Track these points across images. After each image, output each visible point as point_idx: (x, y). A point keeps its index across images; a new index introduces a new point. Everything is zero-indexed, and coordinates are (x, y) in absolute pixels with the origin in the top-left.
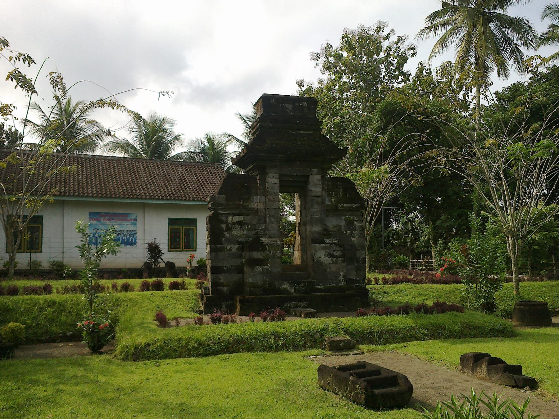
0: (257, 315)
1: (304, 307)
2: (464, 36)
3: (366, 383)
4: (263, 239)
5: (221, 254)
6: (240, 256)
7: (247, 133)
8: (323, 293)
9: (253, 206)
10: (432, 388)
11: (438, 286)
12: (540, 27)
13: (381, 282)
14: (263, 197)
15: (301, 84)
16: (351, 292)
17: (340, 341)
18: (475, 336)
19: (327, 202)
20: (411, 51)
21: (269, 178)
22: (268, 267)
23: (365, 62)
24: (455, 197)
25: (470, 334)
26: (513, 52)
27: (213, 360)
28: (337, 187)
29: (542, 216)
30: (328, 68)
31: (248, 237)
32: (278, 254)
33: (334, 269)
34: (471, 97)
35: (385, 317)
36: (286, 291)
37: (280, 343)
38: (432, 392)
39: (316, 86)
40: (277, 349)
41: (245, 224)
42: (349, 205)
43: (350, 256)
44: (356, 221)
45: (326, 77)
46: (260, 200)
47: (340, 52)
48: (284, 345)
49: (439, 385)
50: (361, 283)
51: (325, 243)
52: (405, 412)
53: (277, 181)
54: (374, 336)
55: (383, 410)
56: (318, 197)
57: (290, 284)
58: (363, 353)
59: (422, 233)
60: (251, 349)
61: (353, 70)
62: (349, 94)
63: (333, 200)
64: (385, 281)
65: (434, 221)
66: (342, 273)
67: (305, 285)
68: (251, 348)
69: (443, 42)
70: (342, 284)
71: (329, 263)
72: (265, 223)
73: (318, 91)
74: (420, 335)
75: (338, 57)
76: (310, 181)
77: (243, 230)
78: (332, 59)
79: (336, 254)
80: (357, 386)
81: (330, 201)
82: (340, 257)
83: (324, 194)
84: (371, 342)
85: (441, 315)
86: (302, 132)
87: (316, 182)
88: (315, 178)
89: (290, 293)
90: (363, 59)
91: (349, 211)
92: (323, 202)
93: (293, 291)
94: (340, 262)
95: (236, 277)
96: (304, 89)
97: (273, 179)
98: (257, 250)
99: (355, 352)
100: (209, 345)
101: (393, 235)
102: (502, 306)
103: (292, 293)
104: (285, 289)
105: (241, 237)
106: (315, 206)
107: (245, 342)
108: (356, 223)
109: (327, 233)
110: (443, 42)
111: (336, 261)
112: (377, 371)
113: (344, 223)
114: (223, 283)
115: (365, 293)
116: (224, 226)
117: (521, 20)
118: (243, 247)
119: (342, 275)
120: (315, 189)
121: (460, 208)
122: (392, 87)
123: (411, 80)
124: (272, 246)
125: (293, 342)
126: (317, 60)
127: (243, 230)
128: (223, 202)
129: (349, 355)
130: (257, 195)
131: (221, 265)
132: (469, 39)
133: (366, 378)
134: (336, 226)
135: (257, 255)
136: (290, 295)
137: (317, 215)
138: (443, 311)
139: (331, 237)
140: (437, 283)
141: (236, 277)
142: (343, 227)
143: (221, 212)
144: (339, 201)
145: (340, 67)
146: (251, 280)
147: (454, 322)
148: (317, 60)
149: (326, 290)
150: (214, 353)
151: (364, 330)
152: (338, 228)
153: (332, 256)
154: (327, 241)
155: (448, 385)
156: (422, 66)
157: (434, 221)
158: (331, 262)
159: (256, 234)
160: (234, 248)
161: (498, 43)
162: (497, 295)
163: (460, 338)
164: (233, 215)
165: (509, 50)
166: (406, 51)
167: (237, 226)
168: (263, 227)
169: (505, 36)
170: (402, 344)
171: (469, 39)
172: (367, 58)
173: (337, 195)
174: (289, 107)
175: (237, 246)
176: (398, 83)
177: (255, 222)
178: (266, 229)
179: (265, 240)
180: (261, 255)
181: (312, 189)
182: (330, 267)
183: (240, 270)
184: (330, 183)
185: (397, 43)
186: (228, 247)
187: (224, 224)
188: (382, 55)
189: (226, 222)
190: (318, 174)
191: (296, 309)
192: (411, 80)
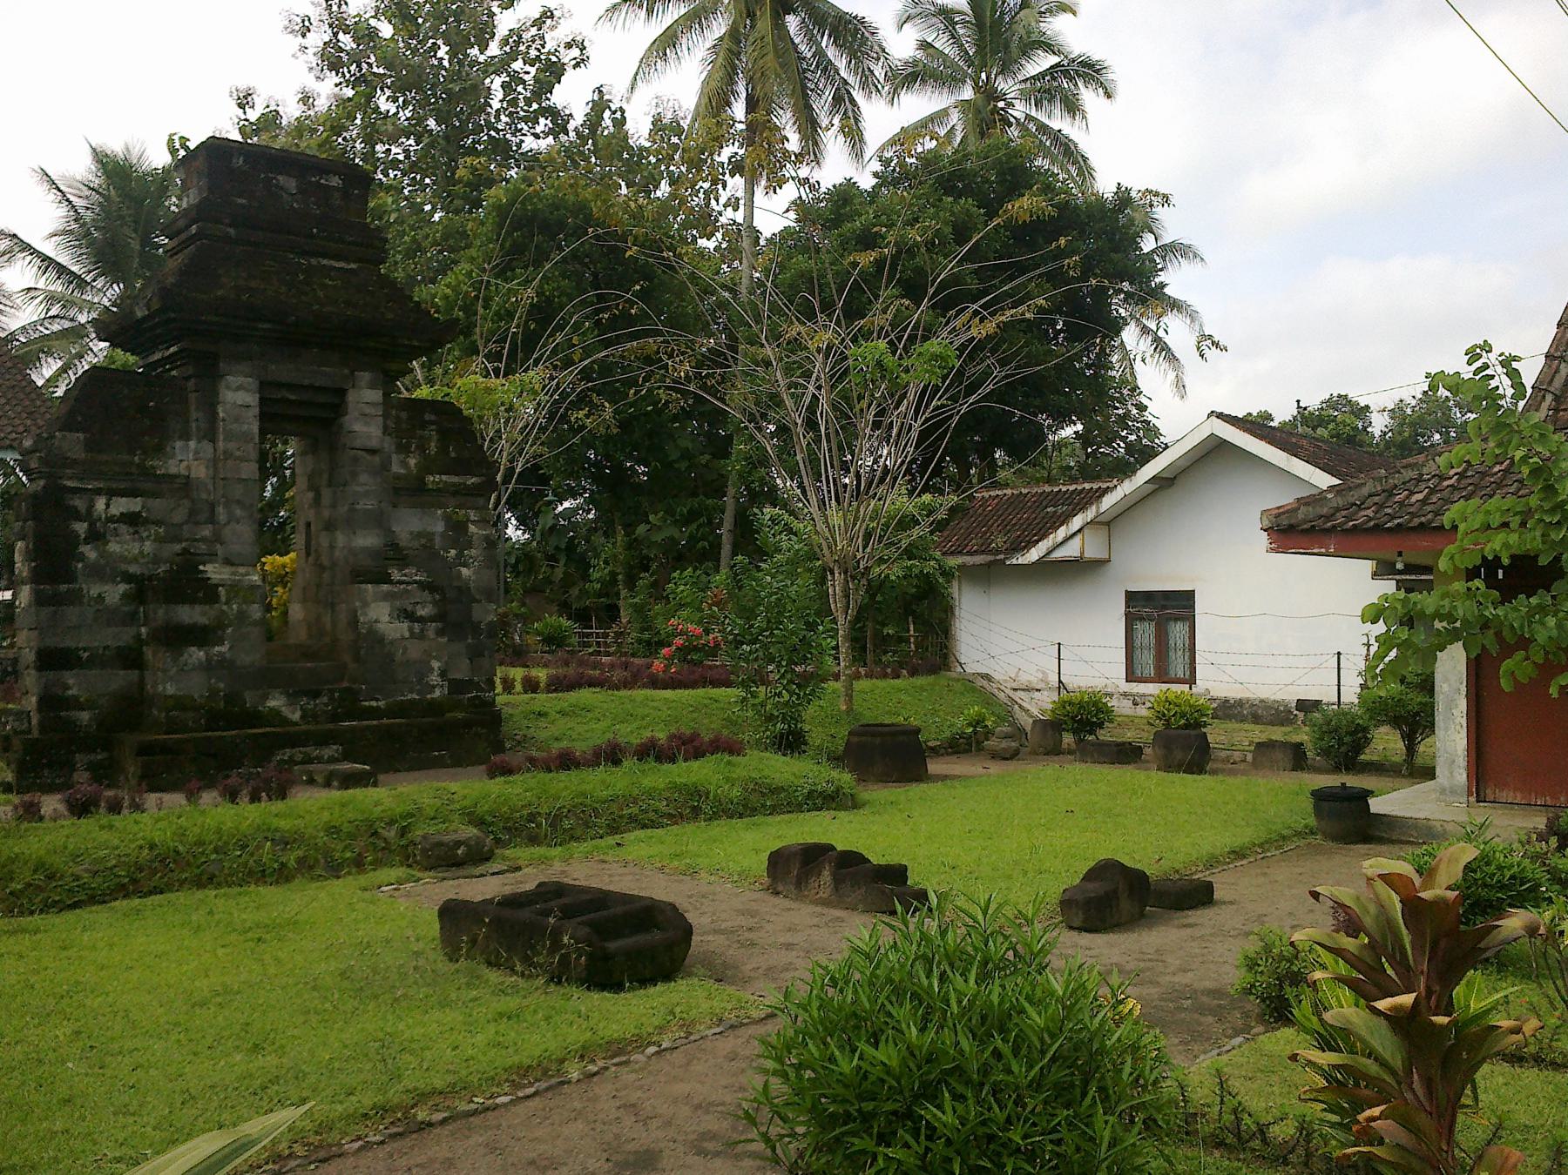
0: (210, 785)
1: (332, 760)
2: (721, 39)
3: (587, 930)
4: (209, 567)
5: (72, 613)
6: (132, 618)
7: (64, 232)
8: (385, 721)
9: (173, 470)
10: (715, 932)
11: (668, 694)
12: (902, 45)
13: (518, 687)
14: (207, 447)
15: (244, 101)
16: (460, 715)
17: (458, 844)
18: (774, 810)
19: (396, 468)
20: (575, 52)
21: (228, 388)
22: (224, 649)
23: (446, 63)
24: (683, 465)
25: (763, 806)
26: (837, 100)
27: (97, 915)
28: (423, 427)
29: (907, 522)
30: (335, 66)
31: (156, 560)
32: (256, 611)
33: (415, 651)
34: (722, 200)
35: (563, 775)
36: (276, 717)
37: (291, 858)
38: (720, 939)
39: (291, 111)
40: (282, 876)
41: (147, 521)
42: (455, 479)
43: (453, 613)
44: (473, 522)
45: (327, 90)
46: (196, 452)
47: (373, 22)
48: (300, 861)
49: (729, 924)
50: (482, 690)
51: (390, 582)
52: (683, 988)
53: (251, 399)
54: (539, 826)
55: (632, 989)
56: (372, 452)
57: (289, 695)
58: (518, 869)
59: (597, 556)
60: (205, 880)
61: (408, 82)
62: (394, 150)
63: (412, 462)
64: (531, 686)
65: (629, 527)
66: (436, 665)
67: (331, 699)
68: (205, 877)
69: (666, 44)
70: (437, 693)
71: (403, 638)
72: (212, 519)
73: (300, 128)
74: (651, 815)
75: (366, 35)
76: (351, 406)
77: (142, 540)
78: (346, 41)
79: (421, 612)
80: (566, 939)
81: (404, 464)
82: (432, 619)
83: (388, 444)
84: (534, 840)
85: (695, 765)
86: (325, 262)
87: (367, 410)
88: (365, 396)
89: (286, 722)
90: (440, 54)
91: (455, 494)
92: (385, 466)
93: (296, 716)
94: (431, 634)
95: (120, 679)
96: (253, 115)
97: (238, 396)
98: (193, 601)
99: (496, 867)
100: (77, 878)
101: (518, 561)
102: (816, 736)
103: (296, 724)
104: (276, 713)
105: (135, 560)
106: (363, 478)
107: (188, 864)
108: (472, 528)
109: (395, 554)
110: (666, 44)
111: (422, 630)
112: (601, 899)
113: (440, 527)
114: (76, 698)
115: (490, 718)
116: (81, 528)
117: (862, 21)
118: (142, 589)
119: (437, 670)
120: (365, 429)
121: (694, 494)
122: (519, 145)
123: (572, 134)
124: (234, 588)
125: (327, 854)
126: (304, 36)
127: (142, 540)
128: (78, 453)
129: (482, 875)
130: (186, 437)
131: (69, 643)
132: (734, 47)
133: (584, 918)
134: (419, 535)
135: (190, 614)
136: (292, 729)
137: (367, 504)
138: (698, 754)
139: (407, 566)
140: (665, 688)
141: (120, 679)
142: (437, 540)
143: (70, 484)
144: (427, 467)
145: (370, 65)
146: (170, 689)
147: (727, 779)
148: (304, 36)
149: (390, 712)
150: (96, 898)
151: (513, 810)
152: (423, 541)
153: (409, 616)
154: (396, 575)
155: (751, 922)
156: (601, 98)
157: (629, 527)
158: (407, 634)
159: (185, 551)
160: (114, 593)
161: (804, 71)
162: (810, 712)
163: (741, 816)
164: (111, 494)
165: (828, 95)
166: (561, 49)
167: (123, 528)
168: (206, 532)
169: (820, 53)
170: (611, 840)
171: (734, 47)
172: (452, 54)
173: (422, 448)
174: (290, 183)
175: (122, 587)
176: (537, 136)
177: (179, 516)
178: (217, 538)
179: (214, 571)
180: (204, 614)
181: (357, 427)
182: (405, 649)
183: (131, 658)
184: (404, 415)
185: (538, 23)
186: (94, 592)
187: (79, 518)
188: (494, 49)
189: (89, 516)
190: (372, 386)
191: (311, 767)
192: (572, 134)
